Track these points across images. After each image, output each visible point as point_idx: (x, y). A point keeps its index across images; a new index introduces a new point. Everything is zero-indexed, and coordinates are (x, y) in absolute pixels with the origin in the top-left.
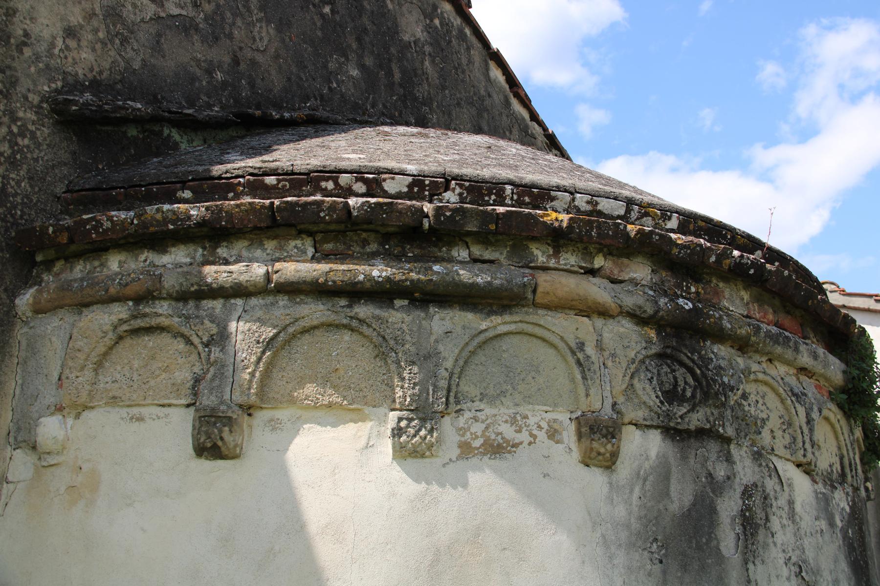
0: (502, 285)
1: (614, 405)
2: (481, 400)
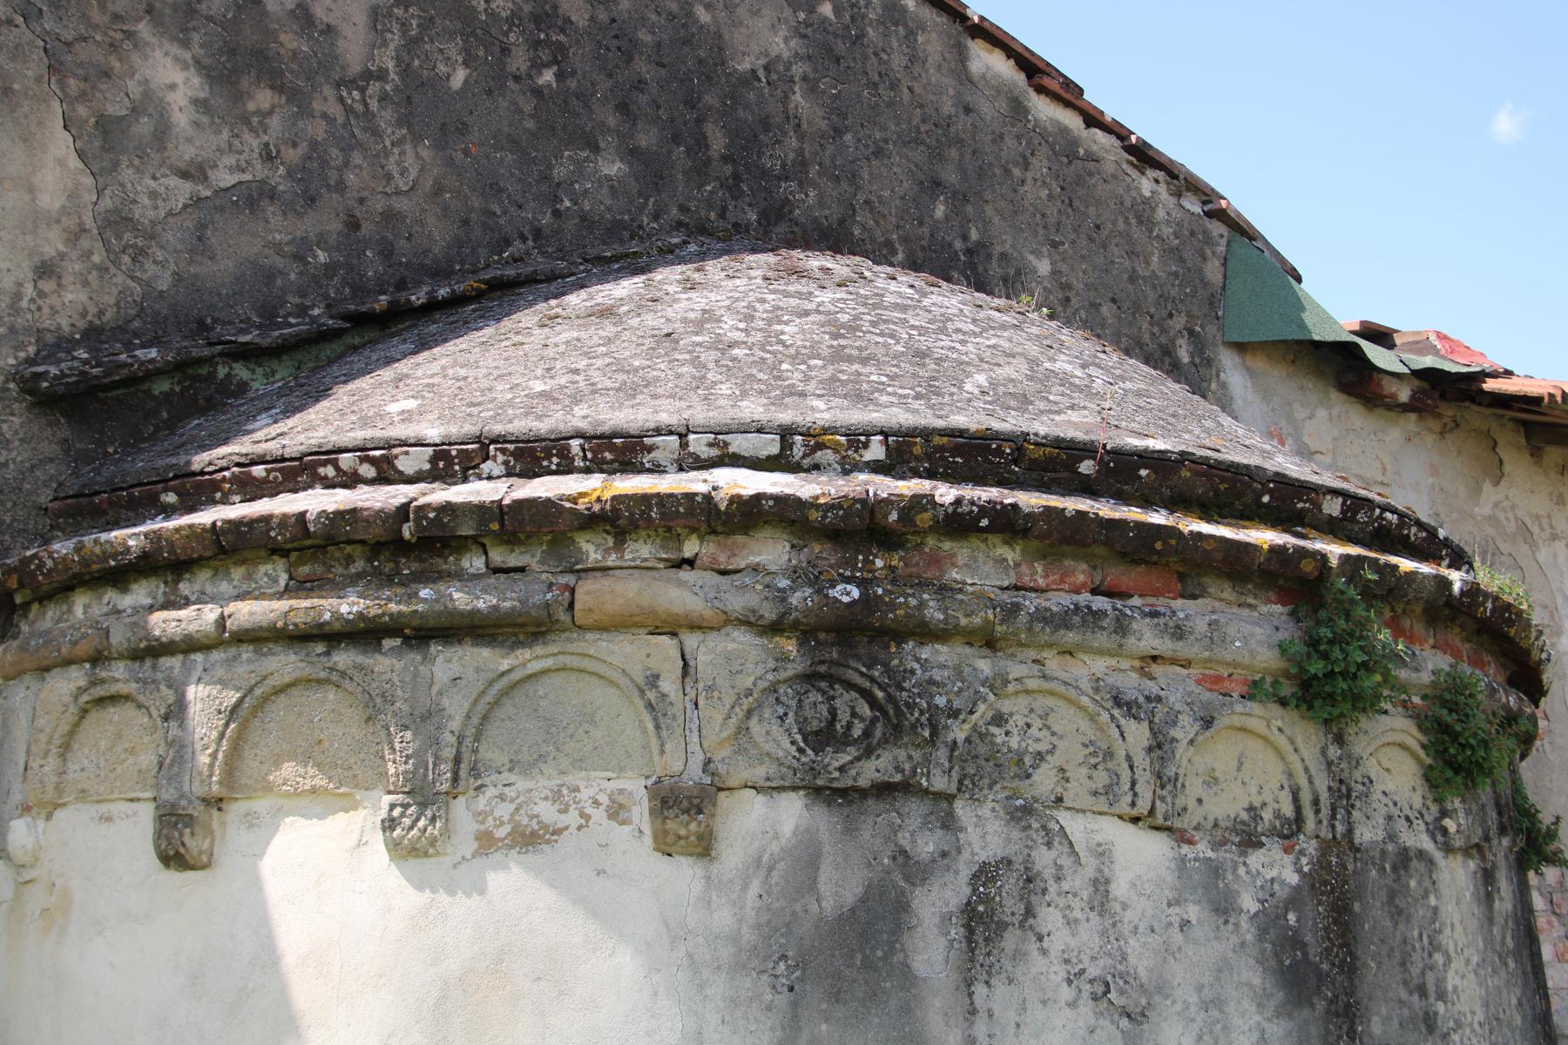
0: (513, 608)
1: (708, 762)
2: (510, 770)
